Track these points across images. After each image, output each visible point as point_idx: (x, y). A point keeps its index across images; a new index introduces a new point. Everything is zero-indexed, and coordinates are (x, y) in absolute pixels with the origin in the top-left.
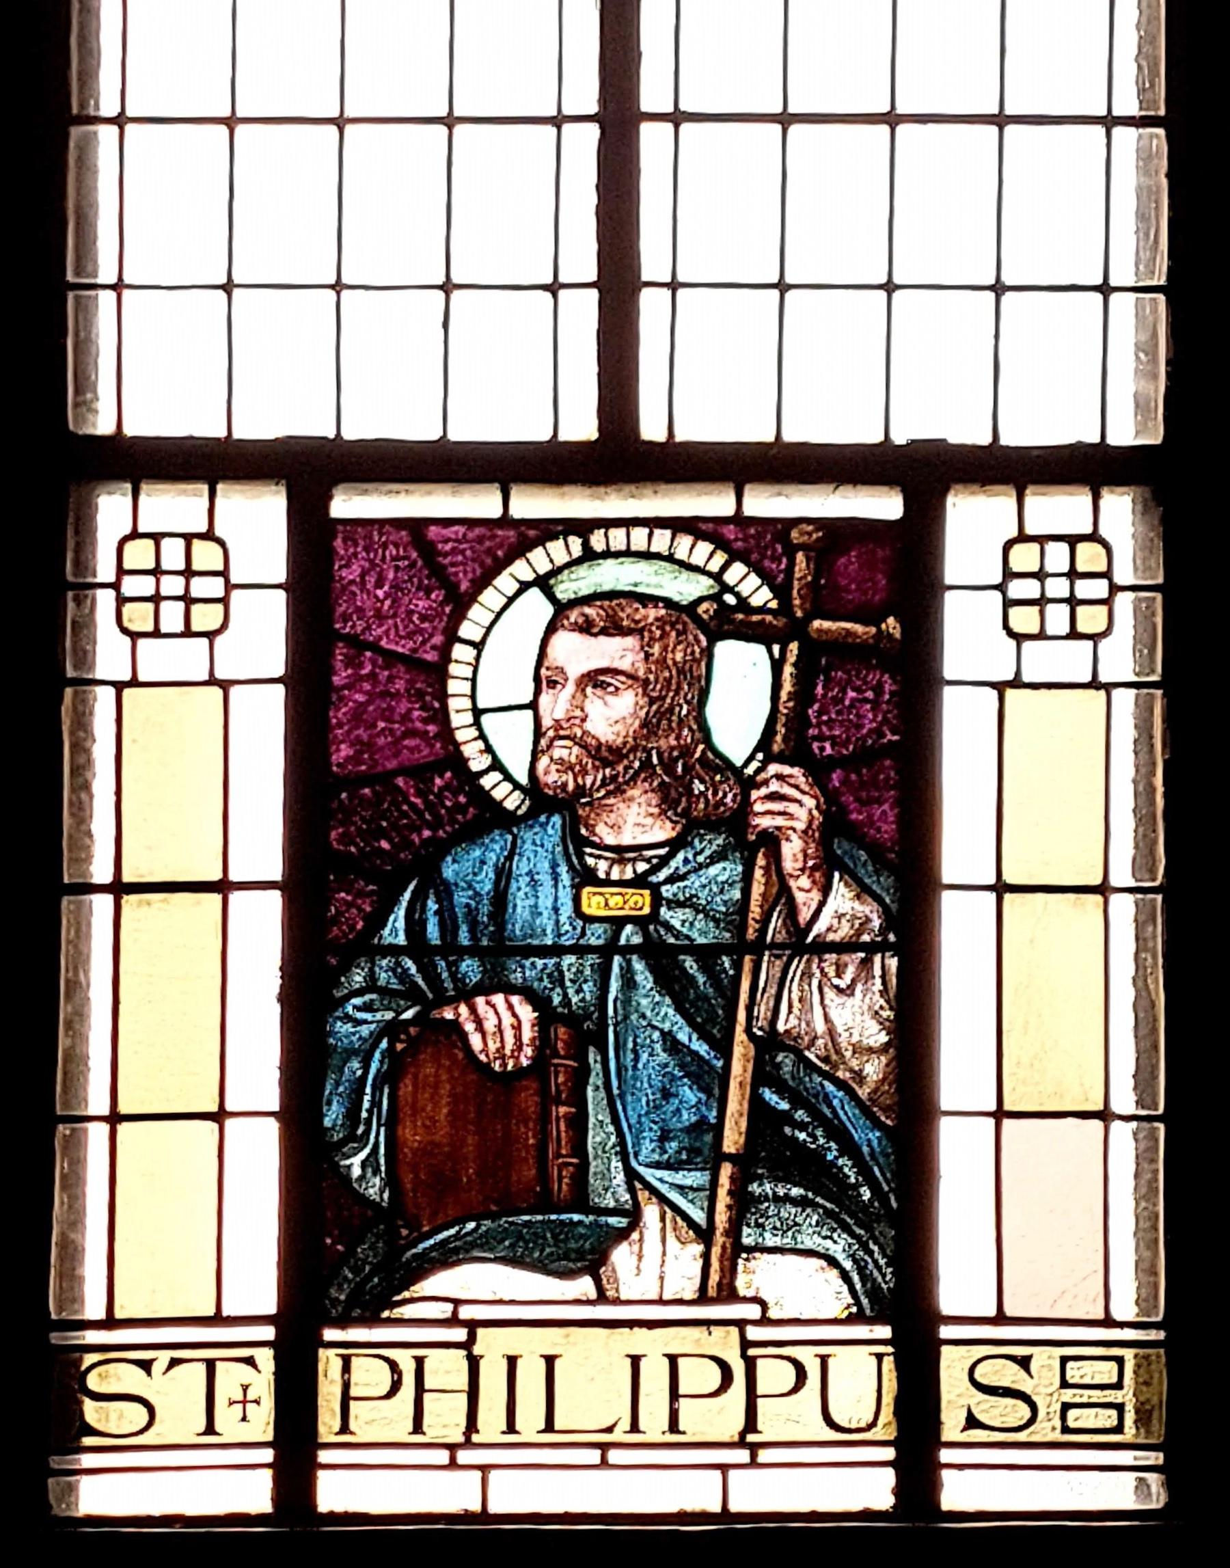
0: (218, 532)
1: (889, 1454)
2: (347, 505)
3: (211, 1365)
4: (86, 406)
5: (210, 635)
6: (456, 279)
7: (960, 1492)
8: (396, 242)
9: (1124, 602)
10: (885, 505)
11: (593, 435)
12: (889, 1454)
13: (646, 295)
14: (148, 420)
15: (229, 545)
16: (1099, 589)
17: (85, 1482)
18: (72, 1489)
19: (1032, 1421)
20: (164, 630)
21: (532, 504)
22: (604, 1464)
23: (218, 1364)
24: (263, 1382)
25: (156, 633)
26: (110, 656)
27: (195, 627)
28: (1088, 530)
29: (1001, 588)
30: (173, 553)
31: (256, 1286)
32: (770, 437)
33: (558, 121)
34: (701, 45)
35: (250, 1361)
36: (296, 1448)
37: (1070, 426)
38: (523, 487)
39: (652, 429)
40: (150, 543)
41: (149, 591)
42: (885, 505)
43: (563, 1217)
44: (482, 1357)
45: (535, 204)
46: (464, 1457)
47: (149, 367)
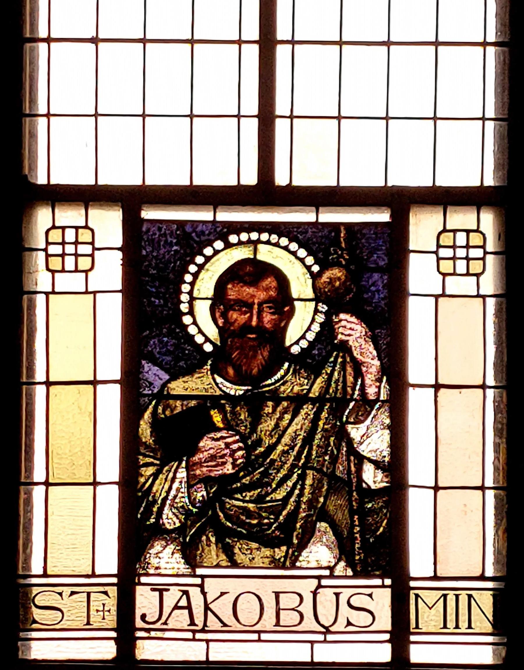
0: (90, 225)
1: (387, 636)
2: (149, 214)
3: (89, 594)
4: (33, 167)
5: (86, 272)
6: (100, 112)
7: (418, 654)
8: (169, 96)
9: (490, 258)
10: (383, 216)
11: (276, 184)
12: (114, 634)
13: (278, 121)
14: (61, 177)
15: (95, 231)
16: (52, 250)
17: (33, 644)
18: (29, 648)
19: (300, 623)
20: (66, 269)
21: (225, 215)
22: (259, 640)
23: (281, 595)
24: (112, 603)
25: (63, 271)
26: (42, 281)
27: (471, 272)
28: (475, 228)
29: (436, 253)
30: (70, 235)
31: (109, 562)
32: (430, 184)
33: (240, 42)
34: (305, 10)
35: (106, 593)
36: (126, 632)
37: (469, 179)
38: (101, 206)
39: (281, 179)
40: (465, 234)
41: (60, 252)
42: (383, 216)
43: (195, 528)
44: (311, 592)
45: (227, 79)
46: (198, 636)
47: (60, 155)
